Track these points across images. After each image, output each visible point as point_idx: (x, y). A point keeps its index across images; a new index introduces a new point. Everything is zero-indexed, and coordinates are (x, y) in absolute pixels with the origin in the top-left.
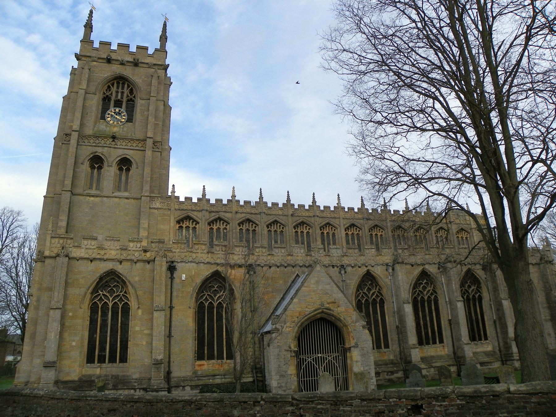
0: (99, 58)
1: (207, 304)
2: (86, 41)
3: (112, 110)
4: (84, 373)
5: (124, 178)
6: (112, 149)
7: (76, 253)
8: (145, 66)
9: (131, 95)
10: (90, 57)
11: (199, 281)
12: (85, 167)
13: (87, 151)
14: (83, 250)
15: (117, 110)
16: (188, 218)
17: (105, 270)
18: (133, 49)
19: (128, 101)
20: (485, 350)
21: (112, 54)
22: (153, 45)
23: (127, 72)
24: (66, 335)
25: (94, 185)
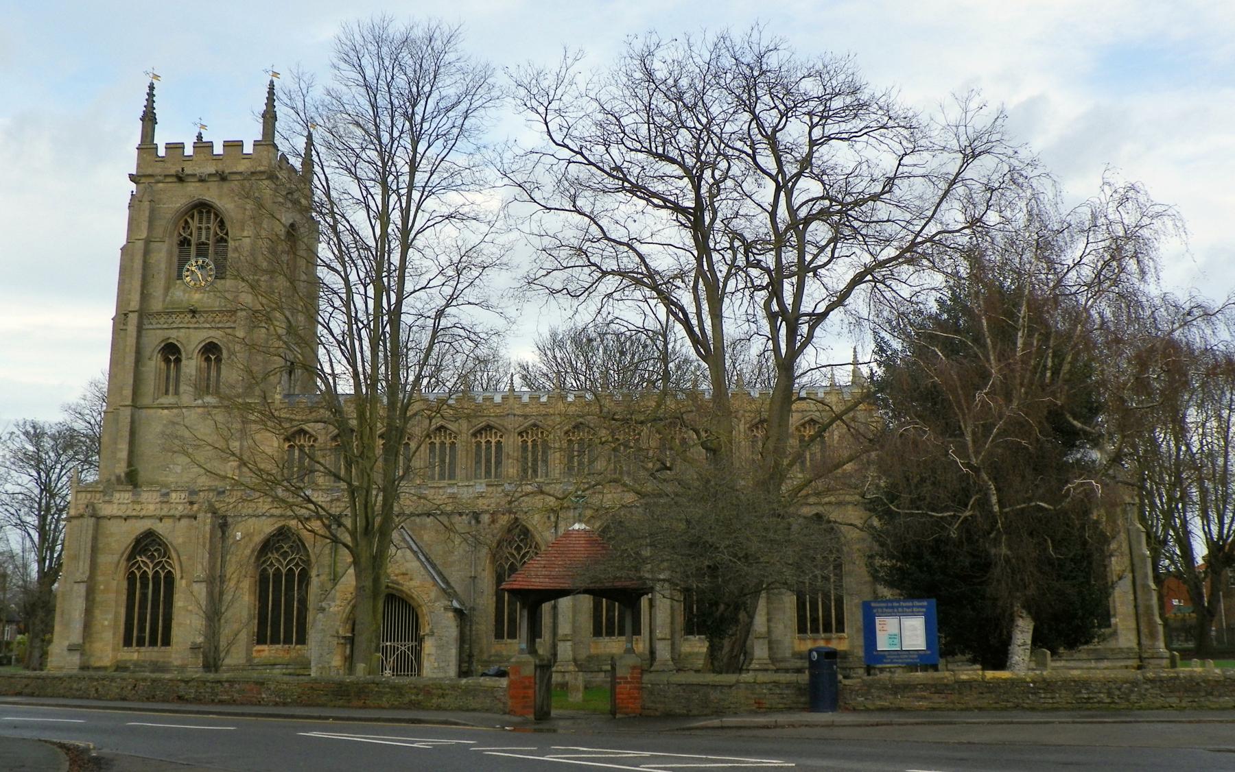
0: (166, 176)
2: (147, 145)
3: (192, 265)
5: (213, 373)
7: (107, 510)
8: (238, 177)
10: (151, 176)
11: (258, 539)
12: (154, 364)
13: (154, 339)
14: (115, 506)
15: (200, 262)
17: (142, 530)
18: (218, 149)
21: (185, 165)
24: (97, 613)
25: (171, 389)
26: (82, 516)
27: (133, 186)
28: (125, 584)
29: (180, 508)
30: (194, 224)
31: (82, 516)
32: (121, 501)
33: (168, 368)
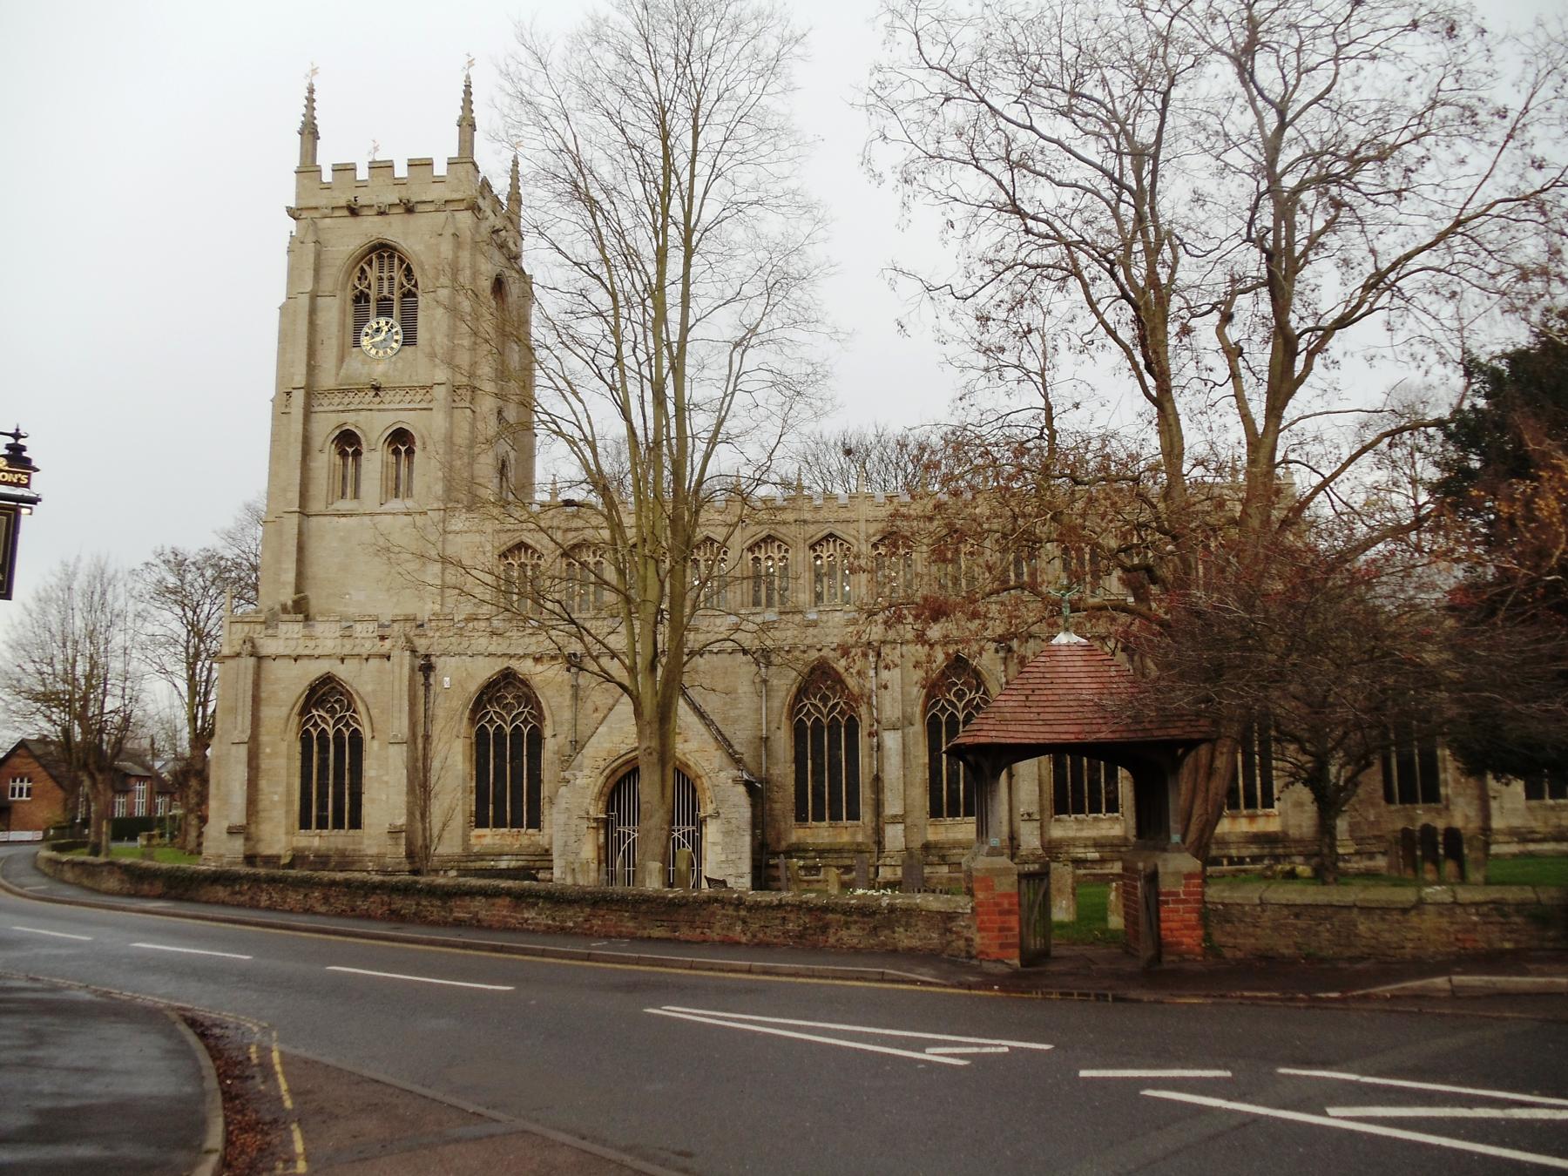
1: (491, 731)
2: (308, 168)
4: (295, 844)
6: (375, 413)
9: (409, 280)
11: (473, 688)
12: (325, 459)
13: (326, 426)
14: (281, 642)
16: (522, 546)
18: (401, 171)
19: (405, 295)
20: (1104, 833)
22: (442, 148)
23: (394, 230)
25: (349, 491)
26: (238, 655)
27: (291, 224)
28: (298, 747)
29: (368, 644)
30: (373, 274)
31: (238, 655)
32: (289, 636)
33: (345, 465)
